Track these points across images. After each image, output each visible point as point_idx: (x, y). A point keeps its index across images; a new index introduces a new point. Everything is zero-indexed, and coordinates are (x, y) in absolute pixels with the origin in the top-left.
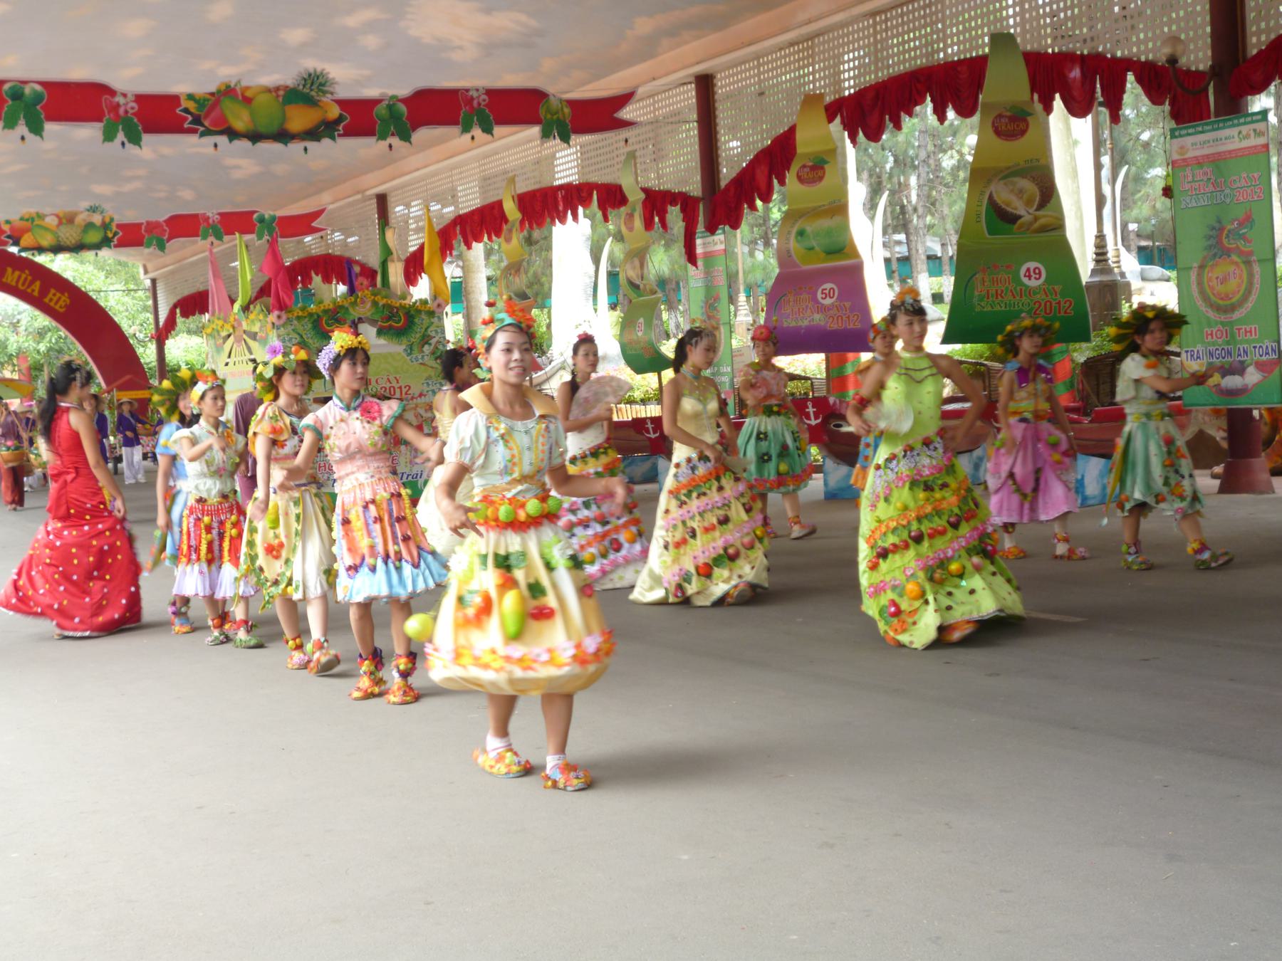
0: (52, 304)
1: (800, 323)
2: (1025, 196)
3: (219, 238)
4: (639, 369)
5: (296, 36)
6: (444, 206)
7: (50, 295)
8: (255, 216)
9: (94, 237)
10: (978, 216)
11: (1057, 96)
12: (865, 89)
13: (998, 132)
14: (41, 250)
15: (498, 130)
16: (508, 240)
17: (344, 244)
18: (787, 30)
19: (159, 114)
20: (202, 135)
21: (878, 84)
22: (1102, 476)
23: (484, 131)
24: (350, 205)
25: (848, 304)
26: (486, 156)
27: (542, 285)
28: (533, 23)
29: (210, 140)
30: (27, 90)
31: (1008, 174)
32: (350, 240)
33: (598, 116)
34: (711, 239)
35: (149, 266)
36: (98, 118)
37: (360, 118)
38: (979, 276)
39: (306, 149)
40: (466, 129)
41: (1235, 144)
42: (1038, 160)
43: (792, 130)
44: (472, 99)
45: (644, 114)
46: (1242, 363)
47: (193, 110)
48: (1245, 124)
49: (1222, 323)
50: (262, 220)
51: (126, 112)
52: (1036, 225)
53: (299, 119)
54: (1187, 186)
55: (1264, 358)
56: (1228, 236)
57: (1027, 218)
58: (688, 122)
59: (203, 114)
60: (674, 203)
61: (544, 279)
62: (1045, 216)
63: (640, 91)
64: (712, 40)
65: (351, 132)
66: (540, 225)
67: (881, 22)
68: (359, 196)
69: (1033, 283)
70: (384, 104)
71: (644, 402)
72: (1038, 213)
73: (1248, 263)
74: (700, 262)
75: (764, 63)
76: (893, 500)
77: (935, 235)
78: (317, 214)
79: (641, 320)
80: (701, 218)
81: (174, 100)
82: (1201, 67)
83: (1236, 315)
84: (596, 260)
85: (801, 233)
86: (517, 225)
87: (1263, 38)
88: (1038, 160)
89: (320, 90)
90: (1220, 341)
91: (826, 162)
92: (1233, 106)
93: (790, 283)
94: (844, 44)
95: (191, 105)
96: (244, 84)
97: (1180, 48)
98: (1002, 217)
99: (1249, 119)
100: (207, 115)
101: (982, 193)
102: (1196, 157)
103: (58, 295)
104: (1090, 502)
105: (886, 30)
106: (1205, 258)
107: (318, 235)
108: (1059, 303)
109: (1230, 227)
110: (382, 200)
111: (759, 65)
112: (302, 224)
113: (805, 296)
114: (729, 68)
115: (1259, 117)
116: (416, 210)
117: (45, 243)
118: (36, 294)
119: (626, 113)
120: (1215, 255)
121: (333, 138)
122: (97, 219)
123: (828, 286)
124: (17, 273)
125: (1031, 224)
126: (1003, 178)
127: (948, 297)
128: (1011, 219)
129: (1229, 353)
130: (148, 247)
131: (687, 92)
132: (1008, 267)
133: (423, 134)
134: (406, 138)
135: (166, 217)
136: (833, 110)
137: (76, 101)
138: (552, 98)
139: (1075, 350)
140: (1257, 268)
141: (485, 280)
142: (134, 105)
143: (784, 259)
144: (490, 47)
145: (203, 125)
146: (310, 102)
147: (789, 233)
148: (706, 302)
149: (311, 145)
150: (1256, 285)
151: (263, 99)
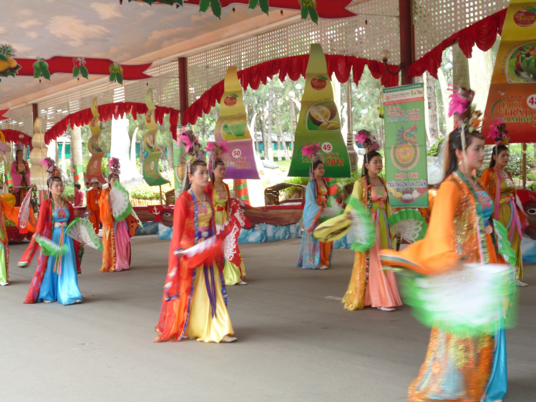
2: (324, 114)
4: (151, 184)
6: (63, 110)
10: (304, 121)
11: (334, 73)
12: (253, 67)
13: (313, 86)
15: (90, 76)
17: (17, 125)
18: (219, 40)
24: (21, 108)
25: (245, 158)
27: (106, 147)
28: (107, 31)
31: (317, 104)
32: (20, 123)
33: (135, 72)
37: (26, 67)
41: (410, 97)
43: (222, 83)
44: (79, 62)
45: (156, 73)
46: (411, 188)
48: (414, 88)
49: (403, 172)
52: (329, 127)
54: (390, 113)
55: (421, 187)
56: (406, 135)
57: (325, 123)
58: (175, 78)
60: (167, 113)
61: (107, 144)
62: (333, 123)
63: (154, 63)
64: (186, 43)
65: (21, 73)
66: (106, 120)
67: (260, 38)
69: (327, 151)
71: (151, 199)
73: (415, 147)
74: (178, 139)
77: (275, 133)
79: (153, 162)
82: (396, 64)
83: (409, 168)
85: (226, 127)
87: (422, 52)
89: (8, 54)
90: (402, 179)
91: (237, 96)
92: (408, 81)
94: (242, 48)
97: (388, 55)
98: (315, 122)
99: (416, 86)
101: (306, 112)
102: (393, 101)
105: (262, 42)
106: (396, 144)
107: (5, 120)
108: (338, 160)
109: (407, 131)
110: (35, 107)
111: (207, 54)
115: (420, 86)
116: (50, 112)
119: (148, 72)
120: (401, 143)
121: (13, 76)
123: (237, 150)
125: (326, 126)
128: (318, 123)
129: (406, 184)
133: (55, 76)
134: (47, 77)
136: (240, 74)
138: (115, 63)
139: (338, 182)
140: (418, 149)
144: (87, 40)
147: (220, 126)
148: (181, 156)
150: (418, 156)
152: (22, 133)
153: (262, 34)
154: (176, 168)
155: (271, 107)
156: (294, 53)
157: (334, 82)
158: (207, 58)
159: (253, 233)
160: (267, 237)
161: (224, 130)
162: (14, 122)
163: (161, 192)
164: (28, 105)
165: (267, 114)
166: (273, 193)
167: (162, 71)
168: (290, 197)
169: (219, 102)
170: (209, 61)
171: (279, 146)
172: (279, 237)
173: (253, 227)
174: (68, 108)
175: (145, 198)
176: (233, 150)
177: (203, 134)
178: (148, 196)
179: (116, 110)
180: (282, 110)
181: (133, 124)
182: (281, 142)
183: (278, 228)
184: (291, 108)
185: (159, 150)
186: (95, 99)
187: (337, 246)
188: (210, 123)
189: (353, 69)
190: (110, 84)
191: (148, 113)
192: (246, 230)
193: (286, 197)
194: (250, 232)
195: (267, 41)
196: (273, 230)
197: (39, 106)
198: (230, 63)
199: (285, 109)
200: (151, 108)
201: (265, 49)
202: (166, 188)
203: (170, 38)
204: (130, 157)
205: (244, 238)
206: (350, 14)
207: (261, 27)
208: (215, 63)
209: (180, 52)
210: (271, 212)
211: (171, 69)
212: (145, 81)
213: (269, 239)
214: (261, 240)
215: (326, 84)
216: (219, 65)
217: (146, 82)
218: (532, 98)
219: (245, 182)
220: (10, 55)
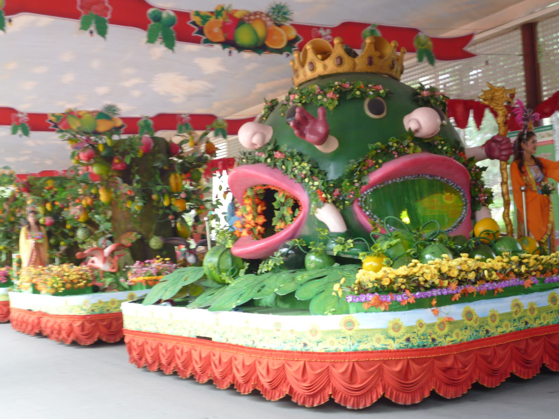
5: (102, 90)
19: (38, 123)
28: (211, 86)
33: (452, 50)
36: (9, 123)
47: (199, 23)
63: (476, 38)
76: (40, 287)
81: (45, 116)
95: (197, 20)
100: (60, 123)
119: (469, 49)
138: (218, 119)
144: (190, 97)
151: (87, 116)
179: (220, 167)
206: (469, 55)
220: (287, 19)
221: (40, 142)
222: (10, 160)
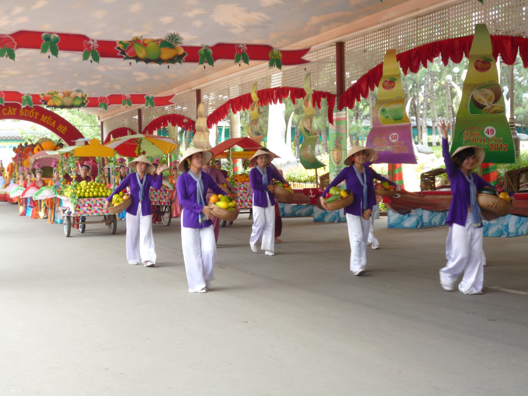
0: (60, 130)
1: (381, 150)
3: (130, 105)
5: (167, 20)
6: (223, 96)
7: (59, 127)
8: (145, 96)
9: (78, 102)
10: (466, 105)
12: (412, 49)
13: (477, 68)
14: (55, 107)
15: (251, 62)
16: (253, 110)
18: (378, 23)
19: (107, 49)
20: (125, 59)
21: (417, 47)
22: (516, 224)
23: (245, 62)
24: (185, 94)
25: (403, 142)
26: (244, 75)
28: (268, 17)
29: (128, 61)
30: (52, 37)
31: (481, 87)
32: (183, 108)
33: (294, 58)
34: (340, 113)
35: (101, 117)
37: (192, 55)
38: (466, 132)
39: (168, 67)
40: (237, 61)
42: (494, 81)
43: (380, 67)
44: (240, 48)
45: (314, 58)
47: (121, 48)
50: (148, 98)
51: (93, 48)
52: (492, 110)
53: (166, 54)
57: (488, 107)
59: (126, 50)
60: (324, 97)
61: (264, 129)
63: (313, 48)
64: (345, 27)
65: (188, 60)
67: (420, 21)
68: (189, 90)
69: (490, 136)
70: (203, 49)
71: (305, 182)
72: (493, 105)
74: (334, 123)
75: (367, 38)
77: (430, 117)
78: (171, 97)
79: (310, 146)
80: (336, 103)
81: (114, 43)
84: (287, 122)
85: (383, 110)
86: (257, 103)
88: (494, 81)
89: (176, 42)
91: (396, 80)
93: (376, 132)
95: (121, 46)
96: (144, 38)
98: (477, 106)
101: (469, 95)
103: (63, 127)
104: (511, 235)
107: (171, 105)
108: (501, 145)
110: (198, 92)
112: (165, 101)
113: (384, 138)
114: (351, 40)
116: (212, 98)
117: (57, 104)
118: (54, 126)
119: (306, 57)
121: (180, 63)
122: (80, 95)
123: (394, 134)
124: (46, 117)
125: (490, 109)
126: (478, 89)
127: (441, 144)
128: (481, 107)
130: (100, 107)
131: (332, 49)
132: (479, 128)
133: (219, 63)
134: (211, 63)
135: (108, 95)
137: (72, 42)
138: (274, 49)
139: (498, 168)
141: (240, 129)
142: (97, 45)
143: (375, 122)
144: (248, 28)
145: (125, 55)
146: (171, 47)
147: (378, 110)
149: (171, 65)
151: (151, 45)
152: (186, 118)
153: (422, 16)
154: (331, 152)
155: (427, 91)
156: (453, 35)
157: (499, 64)
158: (365, 42)
159: (408, 218)
160: (423, 223)
161: (382, 114)
162: (179, 107)
163: (317, 175)
164: (193, 91)
165: (421, 98)
166: (430, 178)
167: (319, 56)
168: (446, 182)
169: (377, 86)
170: (367, 45)
171: (434, 131)
172: (435, 223)
173: (409, 212)
174: (229, 94)
175: (299, 181)
176: (391, 134)
177: (357, 119)
178: (303, 179)
180: (437, 95)
181: (290, 109)
182: (436, 127)
183: (434, 214)
184: (447, 92)
185: (315, 134)
186: (256, 84)
187: (498, 235)
188: (364, 108)
189: (520, 50)
190: (269, 69)
191: (305, 98)
192: (402, 216)
193: (442, 183)
194: (405, 217)
195: (427, 23)
196: (430, 216)
197: (202, 92)
198: (389, 46)
199: (440, 93)
200: (309, 93)
201: (423, 32)
202: (321, 172)
203: (328, 23)
204: (286, 142)
205: (400, 223)
207: (421, 9)
208: (371, 47)
209: (338, 37)
210: (428, 197)
211: (326, 54)
212: (303, 66)
213: (425, 225)
214: (417, 226)
215: (490, 66)
216: (375, 49)
217: (304, 67)
218: (488, 130)
219: (400, 167)
220: (178, 43)
221: (110, 68)
222: (83, 83)
